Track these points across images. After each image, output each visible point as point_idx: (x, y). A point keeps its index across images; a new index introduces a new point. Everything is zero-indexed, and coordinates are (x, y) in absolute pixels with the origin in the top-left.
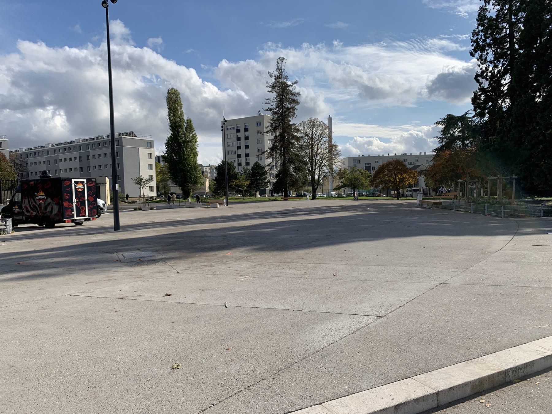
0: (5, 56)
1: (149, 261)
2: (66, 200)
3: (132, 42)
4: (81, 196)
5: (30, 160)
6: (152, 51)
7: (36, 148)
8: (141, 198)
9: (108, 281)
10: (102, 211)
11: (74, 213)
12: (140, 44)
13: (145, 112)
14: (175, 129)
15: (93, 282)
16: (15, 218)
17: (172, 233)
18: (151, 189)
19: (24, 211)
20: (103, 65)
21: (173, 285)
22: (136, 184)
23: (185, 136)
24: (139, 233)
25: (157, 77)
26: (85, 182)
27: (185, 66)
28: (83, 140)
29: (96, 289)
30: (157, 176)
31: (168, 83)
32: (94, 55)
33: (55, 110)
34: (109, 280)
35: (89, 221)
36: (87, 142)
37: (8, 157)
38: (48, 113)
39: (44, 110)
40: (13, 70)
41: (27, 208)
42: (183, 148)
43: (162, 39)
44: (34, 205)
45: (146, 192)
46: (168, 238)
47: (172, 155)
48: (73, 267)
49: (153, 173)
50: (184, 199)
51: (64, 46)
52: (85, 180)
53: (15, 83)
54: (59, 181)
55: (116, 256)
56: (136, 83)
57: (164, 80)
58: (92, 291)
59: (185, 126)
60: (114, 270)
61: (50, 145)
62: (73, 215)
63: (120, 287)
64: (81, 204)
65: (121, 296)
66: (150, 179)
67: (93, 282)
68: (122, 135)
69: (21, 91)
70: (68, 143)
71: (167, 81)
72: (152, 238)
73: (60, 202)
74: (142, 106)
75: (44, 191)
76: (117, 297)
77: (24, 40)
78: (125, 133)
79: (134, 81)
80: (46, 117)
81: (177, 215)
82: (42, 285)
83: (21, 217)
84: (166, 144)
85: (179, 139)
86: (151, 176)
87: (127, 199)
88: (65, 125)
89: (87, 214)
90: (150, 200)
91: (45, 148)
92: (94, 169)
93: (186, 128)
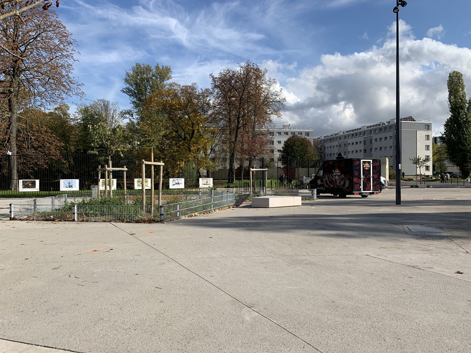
0: (313, 69)
1: (435, 236)
2: (355, 176)
3: (412, 37)
4: (368, 174)
5: (327, 145)
6: (432, 40)
7: (332, 135)
8: (417, 177)
9: (398, 249)
10: (384, 187)
11: (362, 187)
12: (420, 36)
13: (423, 98)
14: (455, 111)
15: (385, 248)
16: (318, 188)
17: (454, 212)
18: (427, 168)
19: (325, 183)
20: (385, 62)
21: (464, 264)
22: (414, 163)
23: (466, 116)
24: (419, 209)
25: (436, 63)
26: (371, 162)
27: (468, 48)
28: (368, 127)
29: (389, 254)
30: (433, 156)
31: (448, 67)
32: (378, 54)
33: (346, 104)
34: (399, 248)
35: (373, 195)
36: (371, 128)
37: (312, 143)
38: (340, 108)
39: (337, 105)
40: (317, 78)
41: (326, 181)
42: (463, 128)
43: (443, 26)
44: (331, 180)
45: (422, 171)
46: (451, 217)
47: (451, 136)
48: (367, 233)
49: (430, 153)
50: (463, 179)
51: (354, 53)
52: (371, 161)
53: (319, 88)
54: (351, 161)
55: (402, 228)
56: (414, 73)
57: (444, 65)
58: (385, 255)
59: (467, 107)
60: (401, 240)
61: (342, 132)
62: (360, 189)
63: (409, 256)
64: (367, 180)
65: (412, 265)
66: (427, 159)
67: (385, 248)
68: (402, 120)
69: (322, 93)
70: (355, 130)
71: (446, 66)
72: (435, 215)
73: (351, 178)
74: (420, 93)
75: (339, 169)
76: (408, 264)
77: (326, 54)
78: (404, 118)
79: (413, 71)
80: (339, 110)
81: (456, 195)
82: (345, 244)
83: (322, 188)
84: (444, 126)
85: (459, 120)
86: (428, 156)
87: (403, 176)
88: (353, 116)
89: (372, 189)
90: (426, 179)
91: (338, 135)
92: (375, 151)
93: (467, 108)
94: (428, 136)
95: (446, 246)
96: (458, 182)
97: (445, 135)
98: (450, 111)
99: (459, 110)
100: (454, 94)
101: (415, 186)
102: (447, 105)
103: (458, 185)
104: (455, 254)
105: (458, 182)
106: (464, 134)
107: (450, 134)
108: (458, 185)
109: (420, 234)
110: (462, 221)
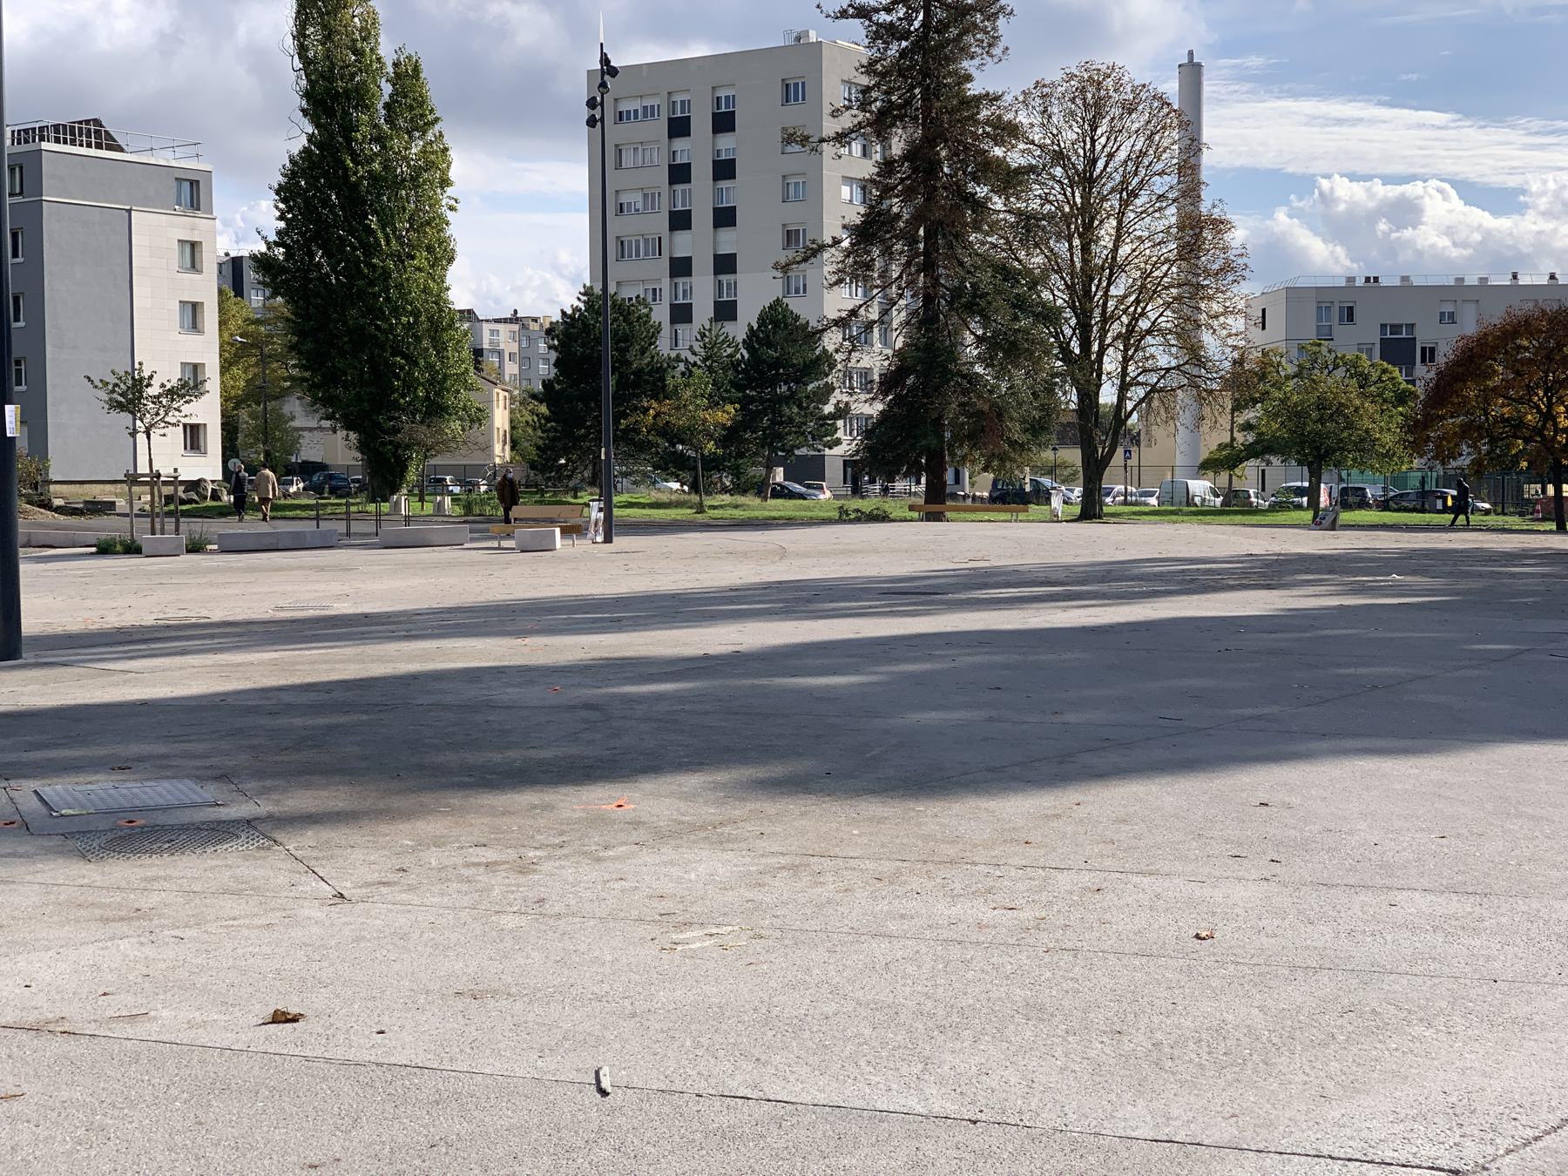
1: (184, 828)
8: (135, 489)
18: (194, 437)
21: (316, 966)
30: (225, 368)
46: (289, 709)
47: (312, 255)
49: (206, 349)
50: (373, 500)
59: (386, 98)
65: (31, 1018)
66: (190, 386)
68: (42, 139)
78: (56, 127)
81: (336, 587)
84: (278, 193)
85: (346, 169)
94: (194, 246)
95: (237, 879)
96: (348, 517)
97: (282, 250)
98: (303, 110)
99: (346, 114)
100: (321, 15)
101: (121, 543)
102: (289, 78)
103: (348, 534)
104: (274, 918)
105: (348, 520)
106: (371, 249)
107: (308, 241)
108: (348, 534)
109: (1105, 519)
110: (337, 726)
